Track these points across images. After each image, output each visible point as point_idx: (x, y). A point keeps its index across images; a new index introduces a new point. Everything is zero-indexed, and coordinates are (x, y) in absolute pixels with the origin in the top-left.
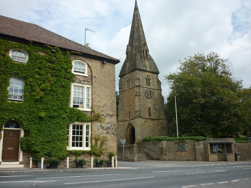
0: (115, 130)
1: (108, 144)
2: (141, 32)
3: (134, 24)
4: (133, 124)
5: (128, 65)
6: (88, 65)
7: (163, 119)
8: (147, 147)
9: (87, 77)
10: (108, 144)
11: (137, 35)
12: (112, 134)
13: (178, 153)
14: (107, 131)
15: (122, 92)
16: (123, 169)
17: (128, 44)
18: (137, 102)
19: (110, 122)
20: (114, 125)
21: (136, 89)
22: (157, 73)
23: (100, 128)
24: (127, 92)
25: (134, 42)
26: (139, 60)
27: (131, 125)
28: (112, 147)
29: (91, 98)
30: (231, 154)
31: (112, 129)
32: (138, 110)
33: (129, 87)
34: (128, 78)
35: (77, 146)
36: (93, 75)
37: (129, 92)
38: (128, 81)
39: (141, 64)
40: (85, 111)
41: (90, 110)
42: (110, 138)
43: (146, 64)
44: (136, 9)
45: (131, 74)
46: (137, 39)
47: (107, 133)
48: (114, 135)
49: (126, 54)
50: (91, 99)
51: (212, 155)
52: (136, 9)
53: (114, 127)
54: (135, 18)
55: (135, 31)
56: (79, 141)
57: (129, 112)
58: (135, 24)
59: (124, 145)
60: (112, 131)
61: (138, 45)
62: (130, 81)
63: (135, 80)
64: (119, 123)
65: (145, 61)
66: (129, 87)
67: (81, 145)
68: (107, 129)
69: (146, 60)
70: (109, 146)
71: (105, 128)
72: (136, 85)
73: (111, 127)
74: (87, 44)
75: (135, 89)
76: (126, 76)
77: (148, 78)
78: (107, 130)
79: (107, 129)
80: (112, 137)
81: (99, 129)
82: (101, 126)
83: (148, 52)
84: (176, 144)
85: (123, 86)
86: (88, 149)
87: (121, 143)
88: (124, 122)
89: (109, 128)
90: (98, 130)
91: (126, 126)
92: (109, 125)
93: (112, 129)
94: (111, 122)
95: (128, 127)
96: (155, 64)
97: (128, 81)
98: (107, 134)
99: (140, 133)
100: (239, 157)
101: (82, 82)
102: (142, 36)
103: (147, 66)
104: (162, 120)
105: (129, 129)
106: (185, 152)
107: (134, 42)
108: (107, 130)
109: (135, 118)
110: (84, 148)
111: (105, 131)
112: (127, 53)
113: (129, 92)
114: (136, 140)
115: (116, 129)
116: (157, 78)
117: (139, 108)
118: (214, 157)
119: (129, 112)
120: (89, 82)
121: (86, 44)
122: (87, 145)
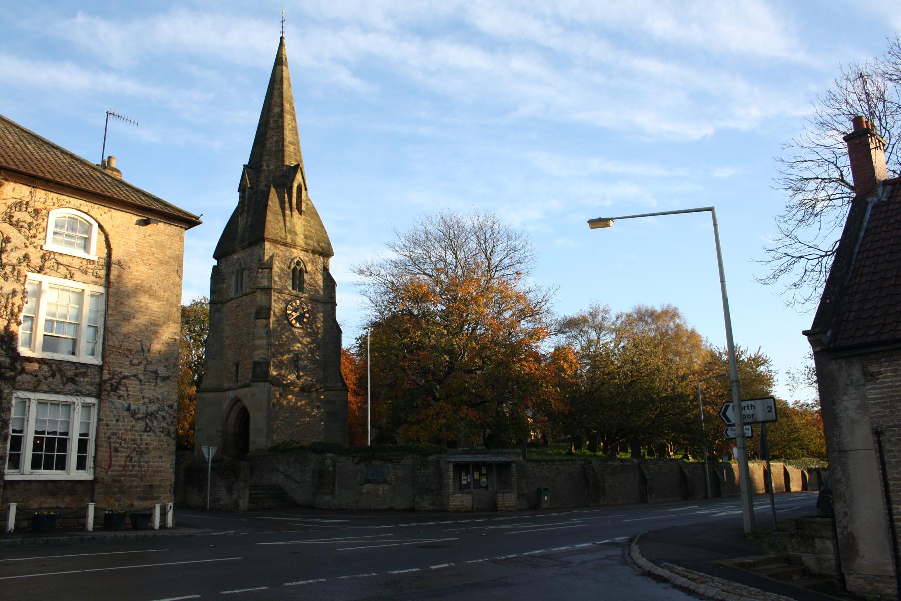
0: (172, 422)
1: (147, 462)
2: (290, 130)
3: (270, 105)
4: (247, 403)
5: (242, 222)
6: (100, 227)
7: (333, 390)
8: (281, 469)
9: (94, 262)
10: (147, 462)
11: (275, 138)
12: (163, 432)
13: (367, 487)
14: (147, 424)
15: (219, 305)
16: (439, 568)
17: (247, 163)
18: (261, 338)
19: (158, 399)
20: (171, 406)
21: (260, 298)
22: (326, 253)
23: (126, 413)
24: (234, 305)
25: (267, 158)
26: (275, 214)
27: (238, 403)
28: (157, 471)
29: (102, 326)
30: (508, 492)
31: (164, 418)
32: (261, 360)
33: (239, 290)
34: (240, 265)
35: (48, 467)
36: (115, 257)
37: (238, 306)
38: (239, 274)
39: (282, 224)
40: (82, 364)
41: (96, 361)
42: (155, 444)
43: (294, 227)
44: (280, 61)
45: (249, 251)
46: (274, 149)
47: (145, 431)
48: (168, 434)
49: (239, 191)
50: (102, 330)
51: (456, 495)
52: (280, 61)
53: (170, 411)
54: (274, 89)
55: (272, 124)
56: (56, 453)
57: (237, 365)
58: (273, 103)
59: (212, 462)
60: (163, 424)
61: (276, 168)
62: (246, 273)
63: (260, 271)
64: (205, 395)
65: (141, 302)
66: (239, 290)
67: (61, 465)
68: (146, 417)
69: (296, 214)
70: (148, 466)
71: (140, 416)
72: (261, 286)
73: (160, 413)
74: (109, 158)
75: (258, 299)
76: (235, 257)
77: (299, 268)
78: (147, 421)
79: (146, 417)
80: (160, 441)
81: (121, 419)
82: (128, 409)
83: (304, 191)
84: (362, 464)
85: (224, 286)
86: (86, 475)
87: (204, 456)
88: (219, 394)
89: (151, 415)
90: (117, 421)
91: (225, 405)
92: (153, 407)
93: (164, 418)
94: (160, 397)
95: (231, 410)
96: (322, 226)
97: (239, 274)
98: (146, 434)
99: (262, 430)
100: (546, 498)
101: (78, 275)
102: (290, 143)
103: (298, 233)
104: (332, 392)
105: (234, 414)
106: (386, 487)
107: (267, 158)
108: (147, 421)
109: (252, 384)
110: (72, 473)
111: (141, 425)
112: (242, 189)
113: (238, 306)
114: (252, 447)
115: (175, 417)
116: (326, 270)
117: (264, 354)
118: (462, 501)
119: (237, 365)
120: (99, 278)
121: (105, 158)
122: (81, 465)
